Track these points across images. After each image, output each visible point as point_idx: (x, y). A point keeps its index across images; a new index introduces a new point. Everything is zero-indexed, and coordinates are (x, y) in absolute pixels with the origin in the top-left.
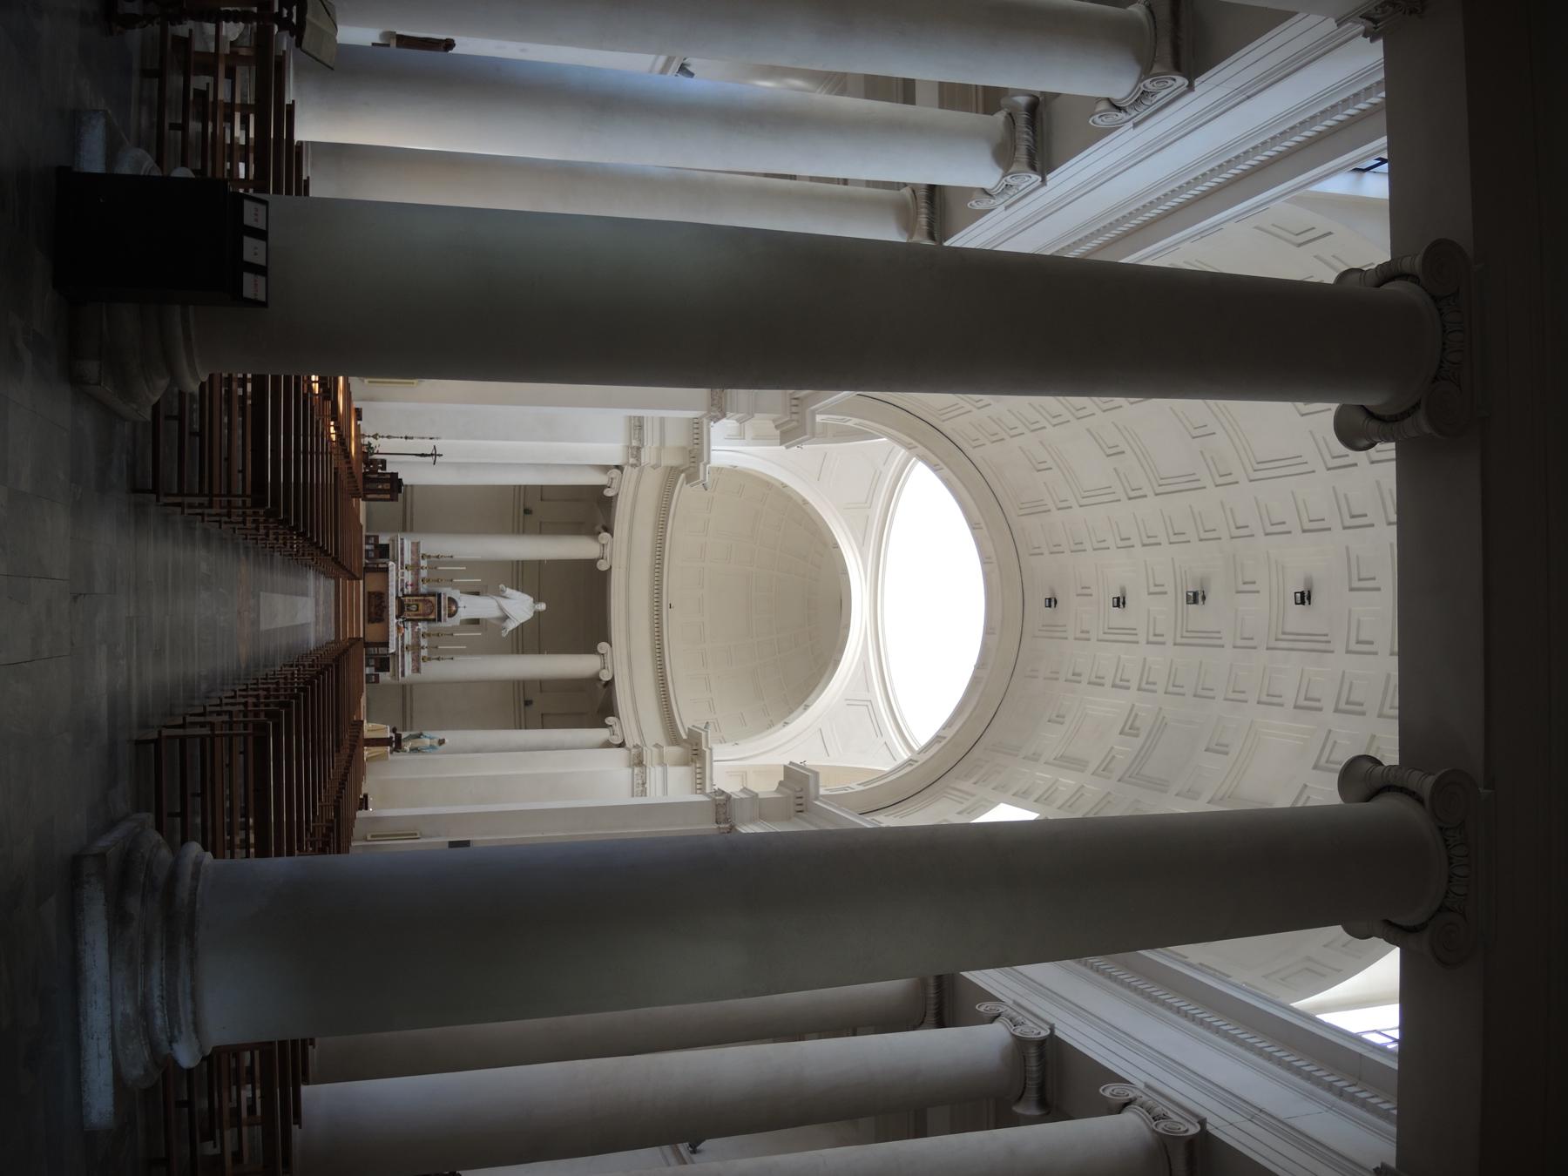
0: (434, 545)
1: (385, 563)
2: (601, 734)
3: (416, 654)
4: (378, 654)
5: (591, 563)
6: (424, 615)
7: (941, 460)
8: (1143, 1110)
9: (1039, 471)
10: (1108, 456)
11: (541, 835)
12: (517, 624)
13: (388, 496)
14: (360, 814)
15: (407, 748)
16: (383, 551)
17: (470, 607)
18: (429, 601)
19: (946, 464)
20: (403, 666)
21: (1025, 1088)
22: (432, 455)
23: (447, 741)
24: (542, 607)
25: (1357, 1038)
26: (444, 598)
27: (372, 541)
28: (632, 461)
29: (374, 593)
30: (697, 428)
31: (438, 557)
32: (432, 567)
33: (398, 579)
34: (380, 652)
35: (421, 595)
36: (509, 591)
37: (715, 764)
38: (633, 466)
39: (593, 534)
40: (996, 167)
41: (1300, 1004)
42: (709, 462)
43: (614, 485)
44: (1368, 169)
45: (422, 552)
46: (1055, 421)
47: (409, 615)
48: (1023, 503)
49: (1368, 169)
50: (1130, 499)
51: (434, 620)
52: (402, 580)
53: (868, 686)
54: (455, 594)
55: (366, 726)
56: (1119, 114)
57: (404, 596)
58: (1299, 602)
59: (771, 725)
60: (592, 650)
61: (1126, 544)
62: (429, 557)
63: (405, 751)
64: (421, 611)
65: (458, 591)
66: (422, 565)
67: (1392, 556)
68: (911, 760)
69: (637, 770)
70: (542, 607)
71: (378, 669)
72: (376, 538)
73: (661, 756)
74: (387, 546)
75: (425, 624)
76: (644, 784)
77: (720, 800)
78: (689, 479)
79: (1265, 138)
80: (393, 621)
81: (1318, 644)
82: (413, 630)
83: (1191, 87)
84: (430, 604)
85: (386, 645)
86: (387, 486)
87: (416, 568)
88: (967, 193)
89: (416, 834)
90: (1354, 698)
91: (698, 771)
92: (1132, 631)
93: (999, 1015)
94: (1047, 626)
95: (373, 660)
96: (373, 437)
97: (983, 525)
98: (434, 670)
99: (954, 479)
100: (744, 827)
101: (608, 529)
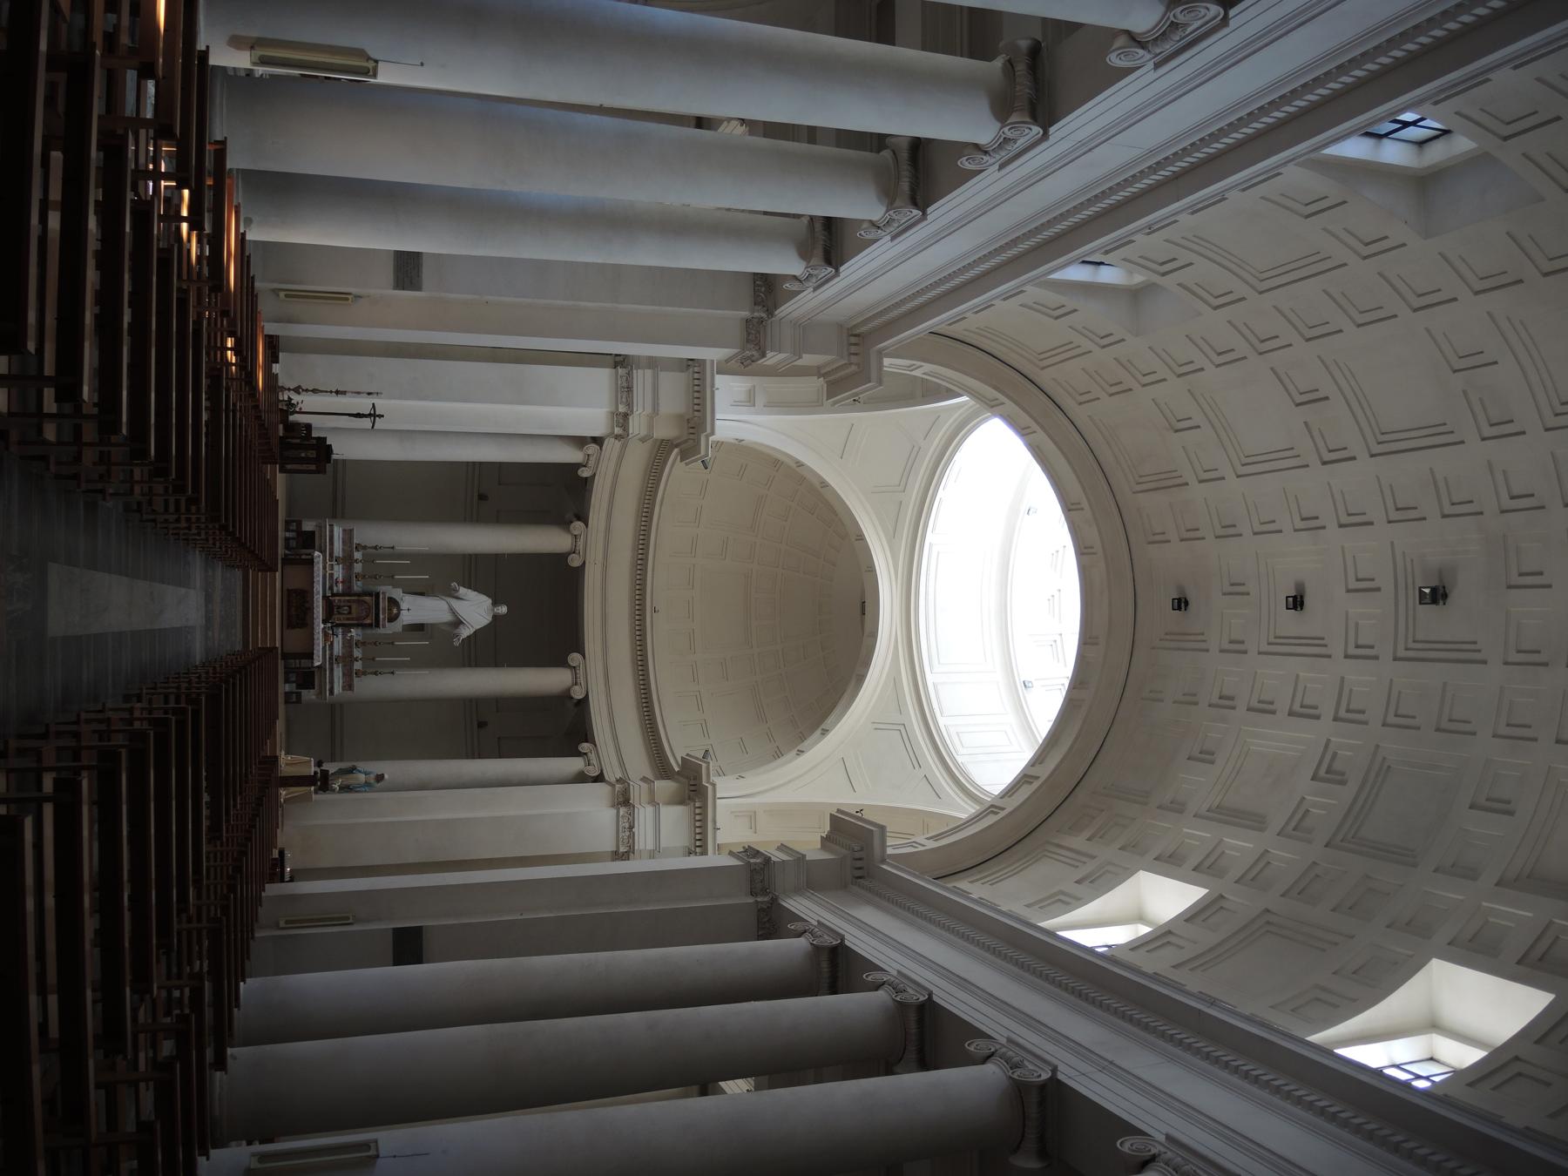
0: (372, 534)
1: (310, 554)
2: (573, 765)
4: (300, 668)
5: (560, 559)
6: (357, 619)
7: (1036, 421)
8: (1002, 1061)
9: (1177, 431)
10: (1298, 405)
11: (520, 917)
12: (472, 631)
13: (313, 467)
14: (272, 890)
15: (336, 786)
16: (308, 540)
17: (419, 609)
18: (366, 603)
19: (1042, 427)
20: (332, 682)
21: (1023, 1136)
22: (370, 415)
23: (386, 776)
24: (503, 609)
25: (1378, 1073)
26: (384, 598)
27: (294, 526)
28: (617, 431)
30: (698, 392)
31: (375, 548)
32: (368, 560)
33: (325, 573)
34: (302, 666)
35: (355, 595)
36: (463, 591)
37: (718, 801)
38: (617, 437)
39: (563, 523)
40: (802, 261)
41: (1315, 1038)
42: (713, 433)
43: (592, 463)
44: (1386, 135)
46: (1114, 389)
48: (1141, 476)
49: (1386, 135)
50: (1324, 463)
52: (331, 575)
53: (901, 708)
54: (397, 594)
55: (284, 758)
56: (984, 157)
57: (334, 595)
58: (1291, 607)
59: (778, 754)
60: (561, 662)
61: (1311, 524)
62: (365, 548)
63: (334, 790)
66: (355, 558)
68: (992, 806)
69: (623, 811)
70: (503, 609)
71: (299, 686)
72: (299, 523)
73: (652, 792)
74: (313, 533)
75: (360, 631)
76: (631, 828)
77: (755, 864)
78: (684, 456)
79: (1342, 61)
80: (319, 626)
81: (1314, 647)
83: (1045, 136)
85: (310, 656)
86: (312, 454)
87: (348, 561)
88: (785, 278)
89: (348, 918)
90: (1307, 702)
91: (698, 811)
92: (1319, 641)
93: (992, 1054)
94: (1171, 634)
95: (294, 675)
96: (293, 390)
97: (1085, 504)
98: (371, 687)
99: (1050, 447)
100: (791, 902)
101: (583, 517)
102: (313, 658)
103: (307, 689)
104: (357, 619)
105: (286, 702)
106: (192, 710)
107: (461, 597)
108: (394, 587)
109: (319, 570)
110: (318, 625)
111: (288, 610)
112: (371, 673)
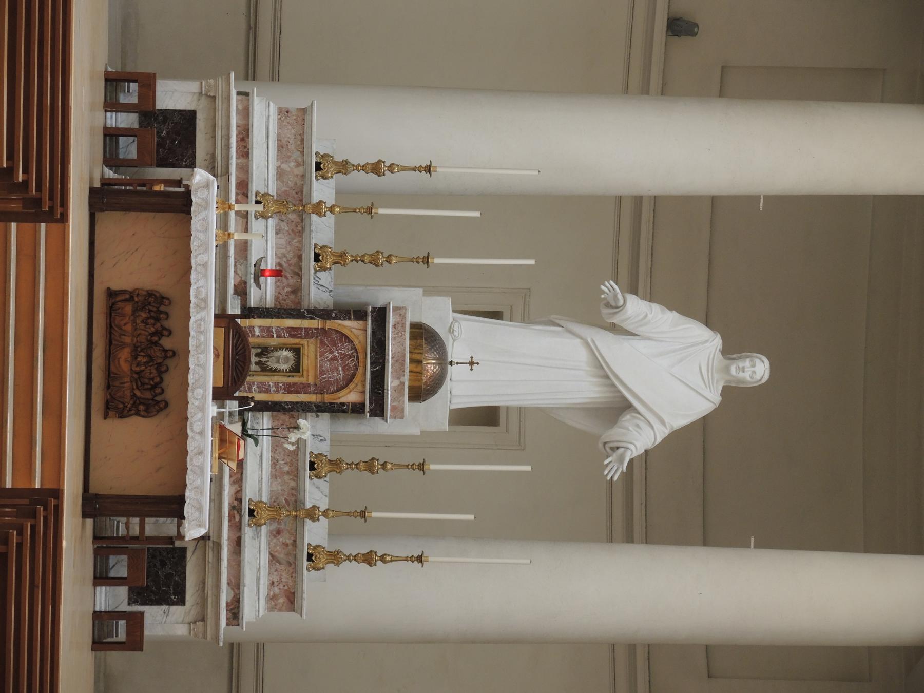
3: (286, 538)
6: (320, 390)
12: (661, 433)
18: (345, 338)
20: (236, 585)
27: (130, 95)
29: (130, 296)
31: (376, 168)
35: (313, 313)
45: (318, 146)
47: (264, 389)
51: (357, 409)
52: (243, 248)
57: (248, 312)
62: (344, 167)
64: (308, 376)
65: (445, 303)
67: (469, 320)
71: (140, 595)
72: (147, 84)
74: (189, 117)
82: (275, 447)
84: (346, 349)
102: (182, 517)
103: (158, 603)
104: (320, 390)
105: (99, 644)
106: (31, 525)
107: (630, 328)
108: (430, 291)
109: (206, 230)
110: (202, 409)
111: (109, 356)
112: (356, 558)
